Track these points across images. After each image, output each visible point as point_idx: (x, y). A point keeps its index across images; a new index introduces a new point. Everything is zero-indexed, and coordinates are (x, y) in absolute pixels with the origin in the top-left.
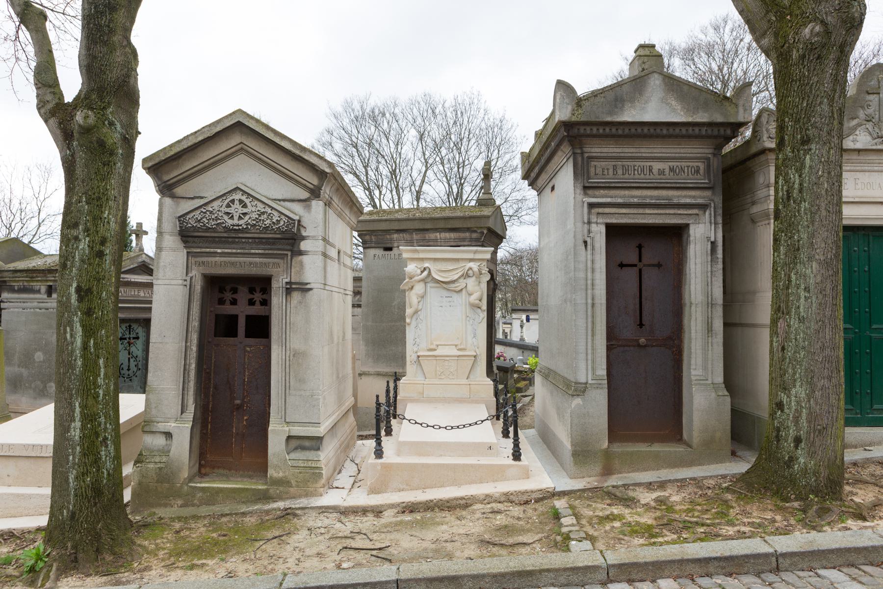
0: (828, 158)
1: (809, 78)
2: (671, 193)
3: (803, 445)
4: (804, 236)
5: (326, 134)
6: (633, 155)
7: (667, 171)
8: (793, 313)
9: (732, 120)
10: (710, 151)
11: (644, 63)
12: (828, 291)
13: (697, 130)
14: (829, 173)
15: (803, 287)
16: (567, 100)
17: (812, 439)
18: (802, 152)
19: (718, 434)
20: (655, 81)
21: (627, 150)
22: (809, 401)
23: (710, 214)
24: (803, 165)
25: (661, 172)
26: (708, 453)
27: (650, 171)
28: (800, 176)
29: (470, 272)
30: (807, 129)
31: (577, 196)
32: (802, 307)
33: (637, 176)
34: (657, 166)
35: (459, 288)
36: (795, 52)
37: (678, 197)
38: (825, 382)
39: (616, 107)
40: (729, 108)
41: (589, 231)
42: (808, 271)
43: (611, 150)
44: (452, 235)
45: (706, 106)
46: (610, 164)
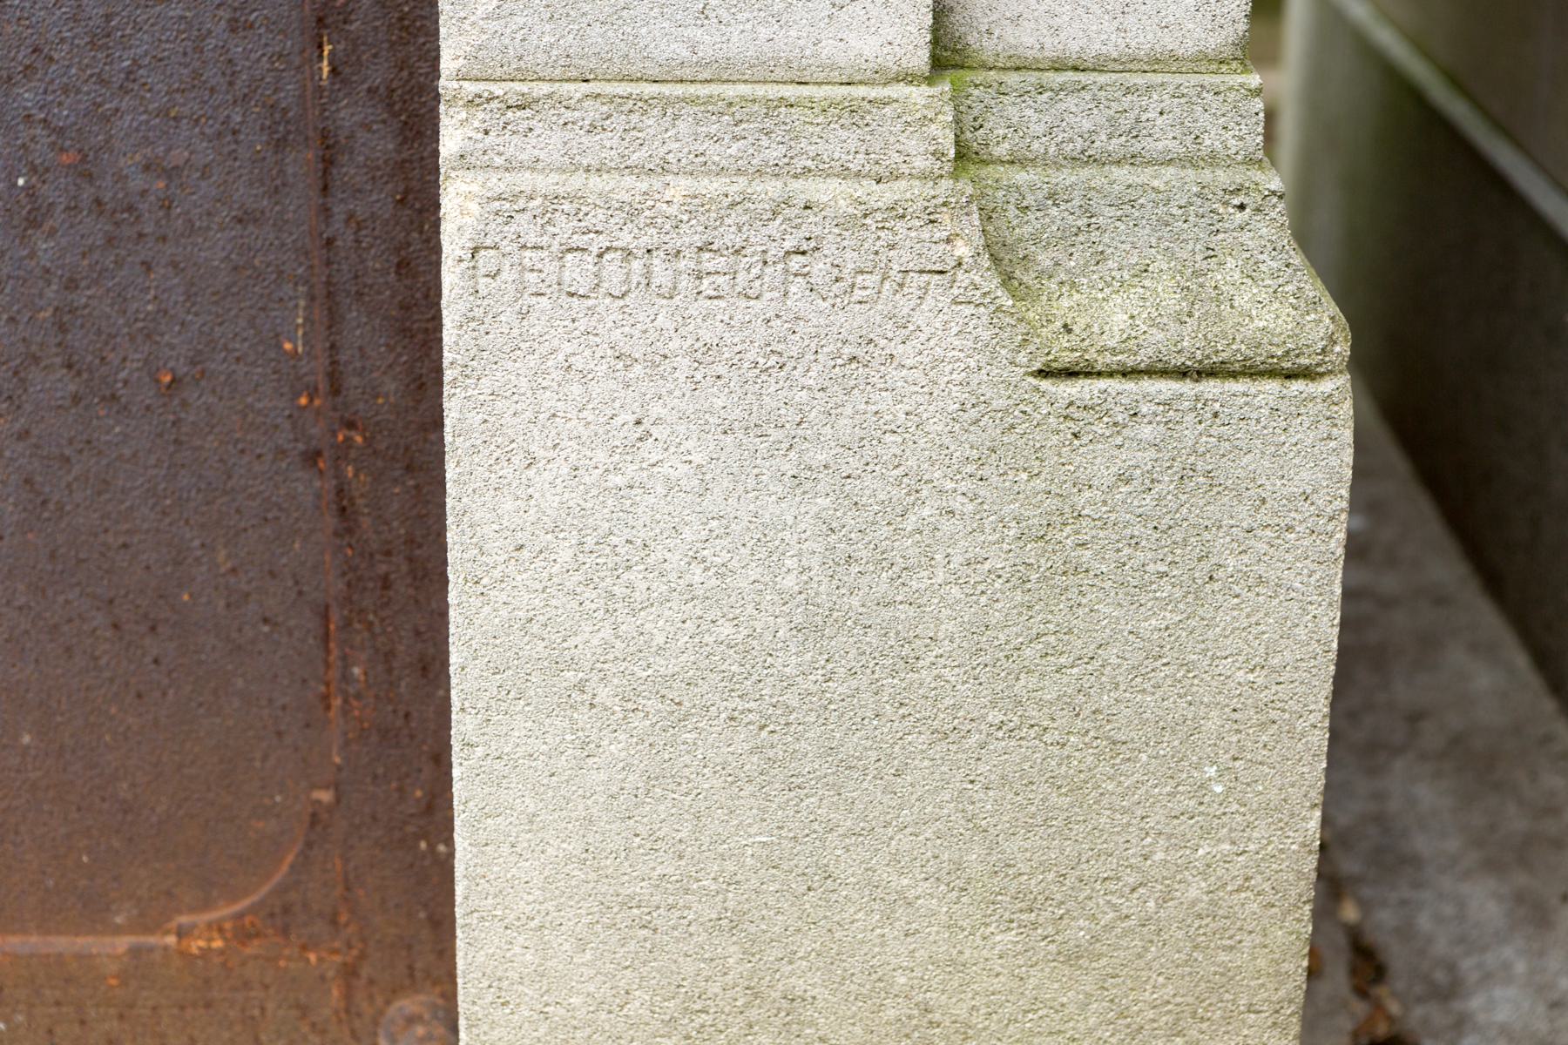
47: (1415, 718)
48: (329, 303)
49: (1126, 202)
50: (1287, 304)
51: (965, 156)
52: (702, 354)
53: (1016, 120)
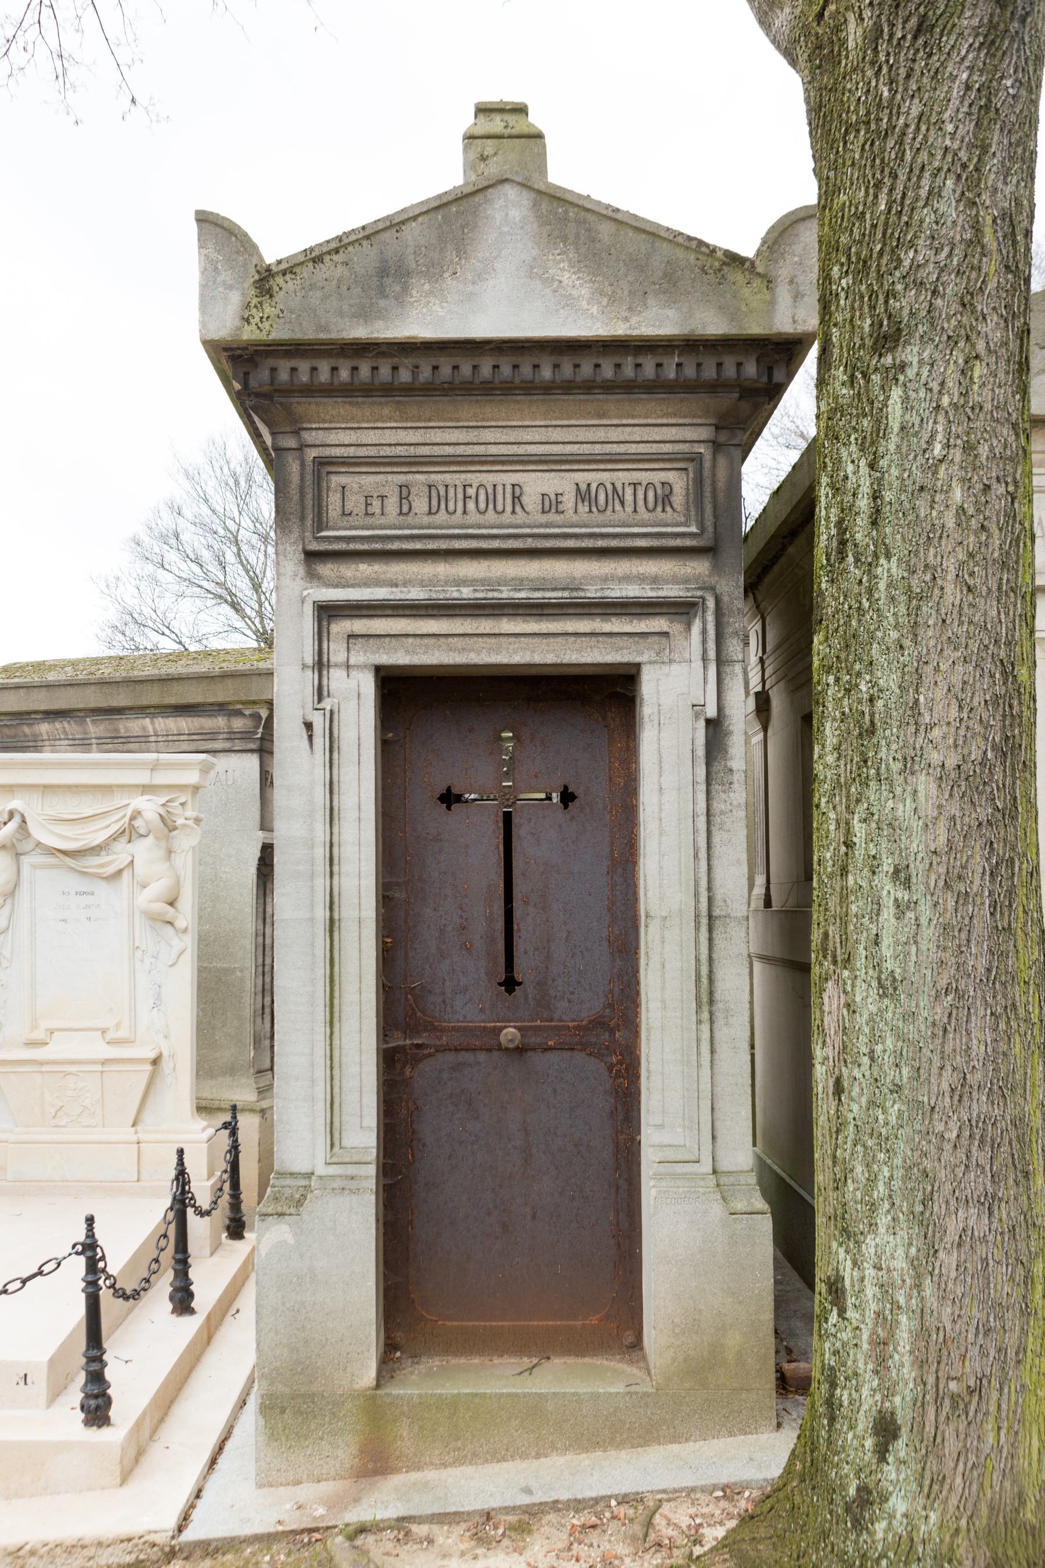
0: (964, 395)
1: (894, 109)
2: (580, 568)
3: (900, 1447)
4: (889, 680)
5: (165, 514)
6: (460, 450)
7: (569, 500)
8: (860, 962)
9: (755, 328)
10: (704, 433)
11: (483, 158)
12: (977, 882)
13: (649, 364)
14: (969, 448)
15: (887, 866)
16: (226, 276)
17: (930, 1429)
18: (876, 378)
19: (734, 1340)
20: (509, 209)
21: (438, 436)
22: (918, 1286)
23: (704, 632)
24: (880, 430)
25: (551, 504)
26: (695, 1403)
27: (517, 499)
28: (872, 466)
29: (138, 823)
30: (890, 294)
31: (286, 581)
32: (886, 941)
33: (473, 517)
34: (536, 485)
35: (110, 870)
36: (852, 25)
37: (605, 579)
38: (973, 1217)
39: (382, 293)
40: (746, 292)
41: (320, 694)
42: (904, 810)
43: (390, 437)
44: (184, 724)
45: (670, 286)
46: (389, 482)
47: (795, 1312)
48: (617, 1212)
49: (739, 1190)
50: (760, 1203)
51: (718, 1185)
52: (685, 1212)
53: (724, 1180)
